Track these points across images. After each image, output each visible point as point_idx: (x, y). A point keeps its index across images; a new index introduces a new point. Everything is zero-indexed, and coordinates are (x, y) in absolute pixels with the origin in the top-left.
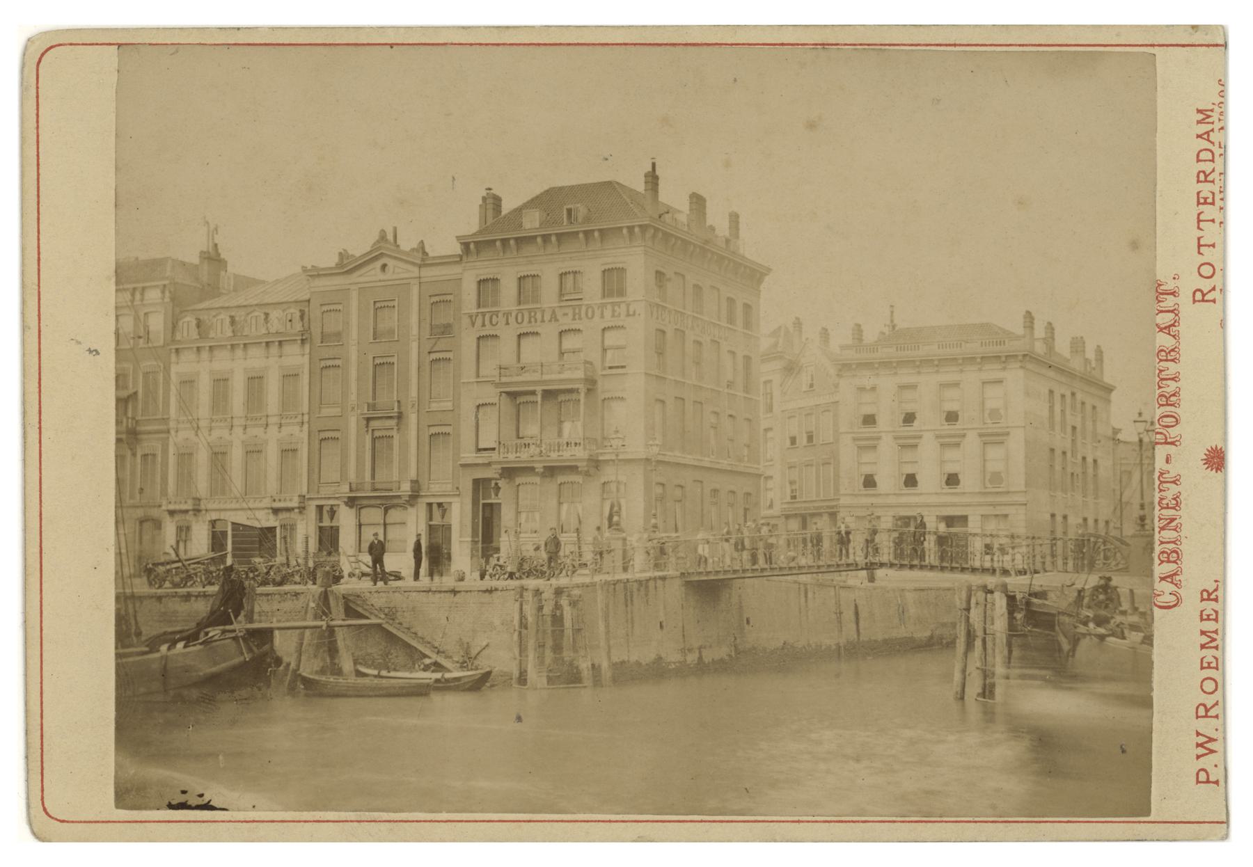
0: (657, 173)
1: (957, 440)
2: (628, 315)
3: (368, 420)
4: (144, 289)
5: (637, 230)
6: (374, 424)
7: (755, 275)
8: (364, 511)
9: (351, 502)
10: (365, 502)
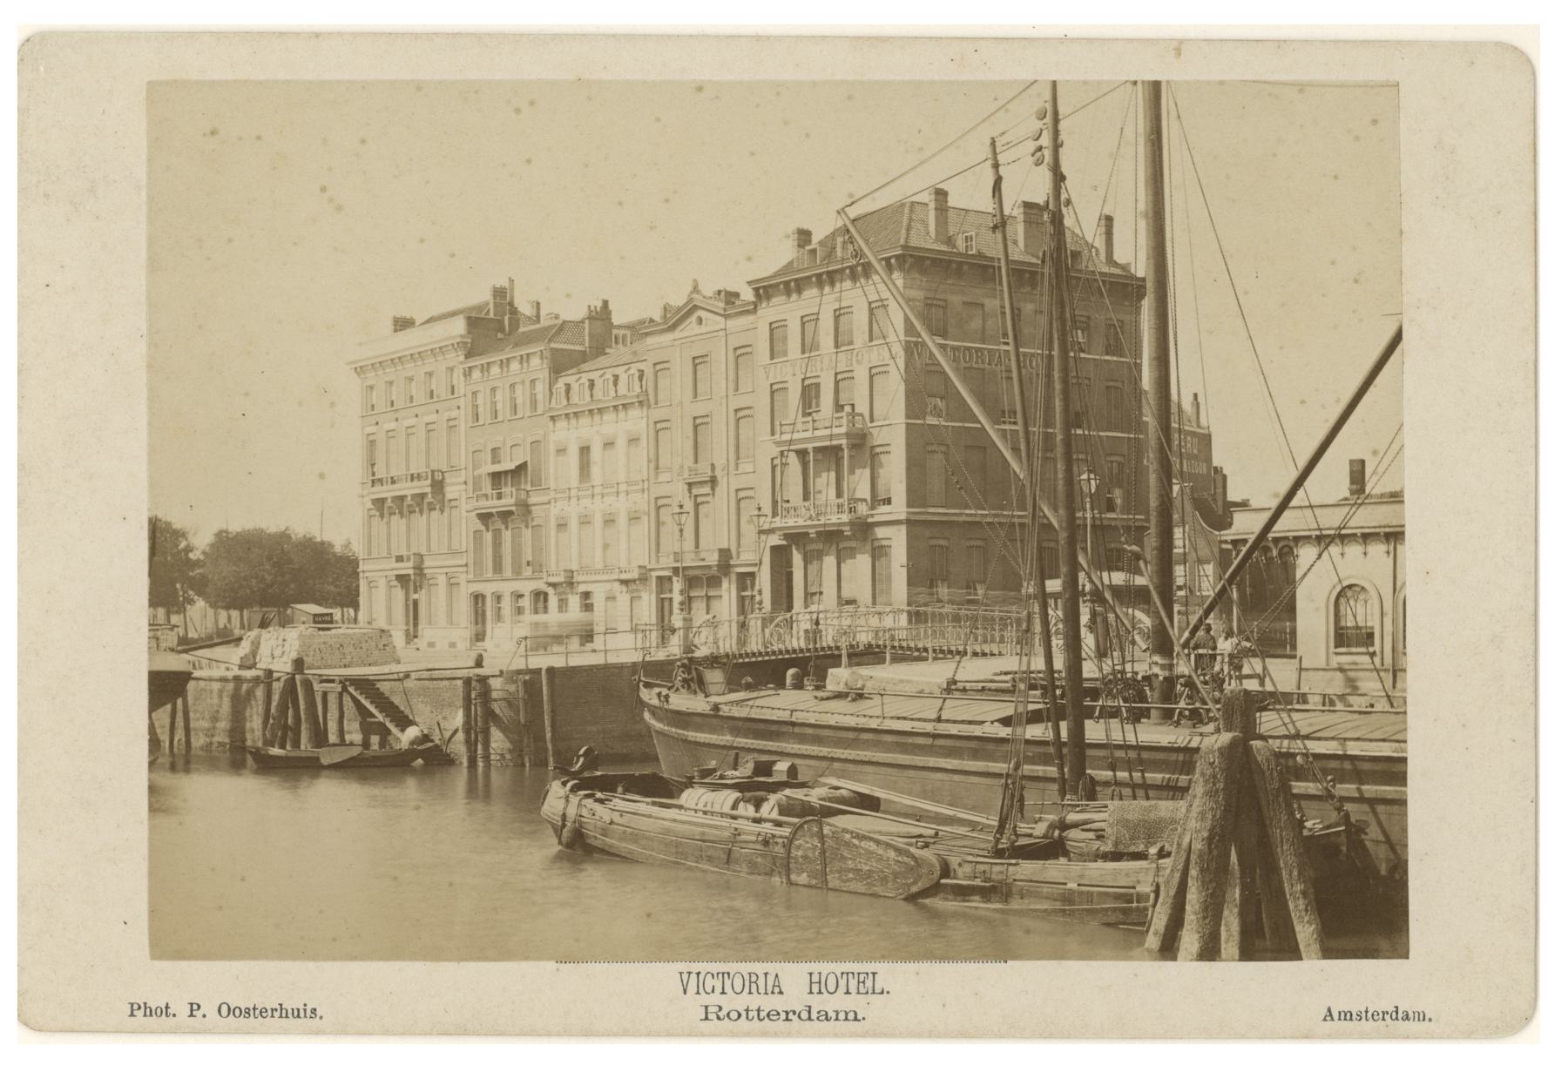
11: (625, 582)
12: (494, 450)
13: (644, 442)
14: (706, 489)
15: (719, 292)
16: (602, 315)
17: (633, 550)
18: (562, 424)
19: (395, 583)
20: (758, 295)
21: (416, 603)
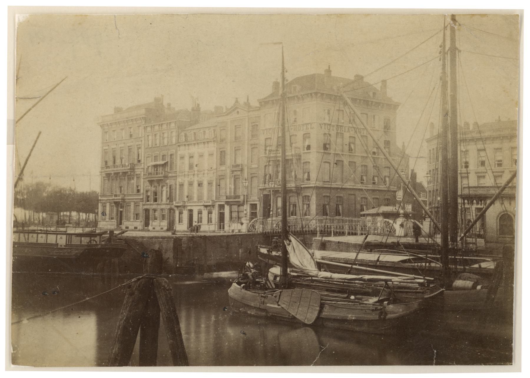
0: (331, 69)
1: (500, 174)
2: (311, 128)
3: (232, 171)
4: (162, 124)
5: (313, 94)
6: (235, 173)
7: (393, 107)
8: (233, 206)
9: (227, 203)
10: (232, 203)
11: (206, 206)
12: (163, 156)
13: (215, 156)
14: (239, 173)
15: (385, 132)
16: (197, 109)
17: (207, 194)
18: (182, 148)
19: (113, 204)
20: (261, 105)
21: (121, 212)
